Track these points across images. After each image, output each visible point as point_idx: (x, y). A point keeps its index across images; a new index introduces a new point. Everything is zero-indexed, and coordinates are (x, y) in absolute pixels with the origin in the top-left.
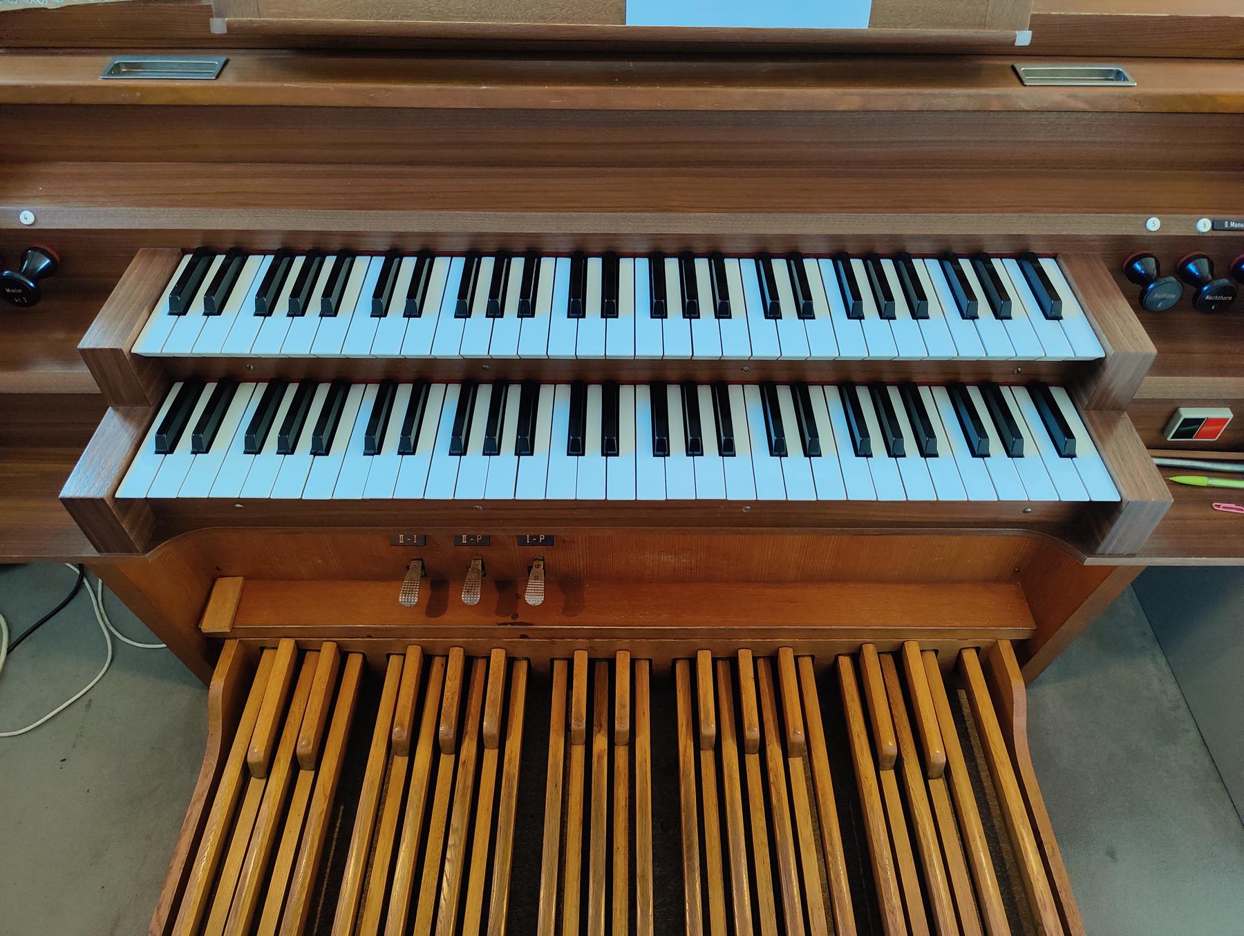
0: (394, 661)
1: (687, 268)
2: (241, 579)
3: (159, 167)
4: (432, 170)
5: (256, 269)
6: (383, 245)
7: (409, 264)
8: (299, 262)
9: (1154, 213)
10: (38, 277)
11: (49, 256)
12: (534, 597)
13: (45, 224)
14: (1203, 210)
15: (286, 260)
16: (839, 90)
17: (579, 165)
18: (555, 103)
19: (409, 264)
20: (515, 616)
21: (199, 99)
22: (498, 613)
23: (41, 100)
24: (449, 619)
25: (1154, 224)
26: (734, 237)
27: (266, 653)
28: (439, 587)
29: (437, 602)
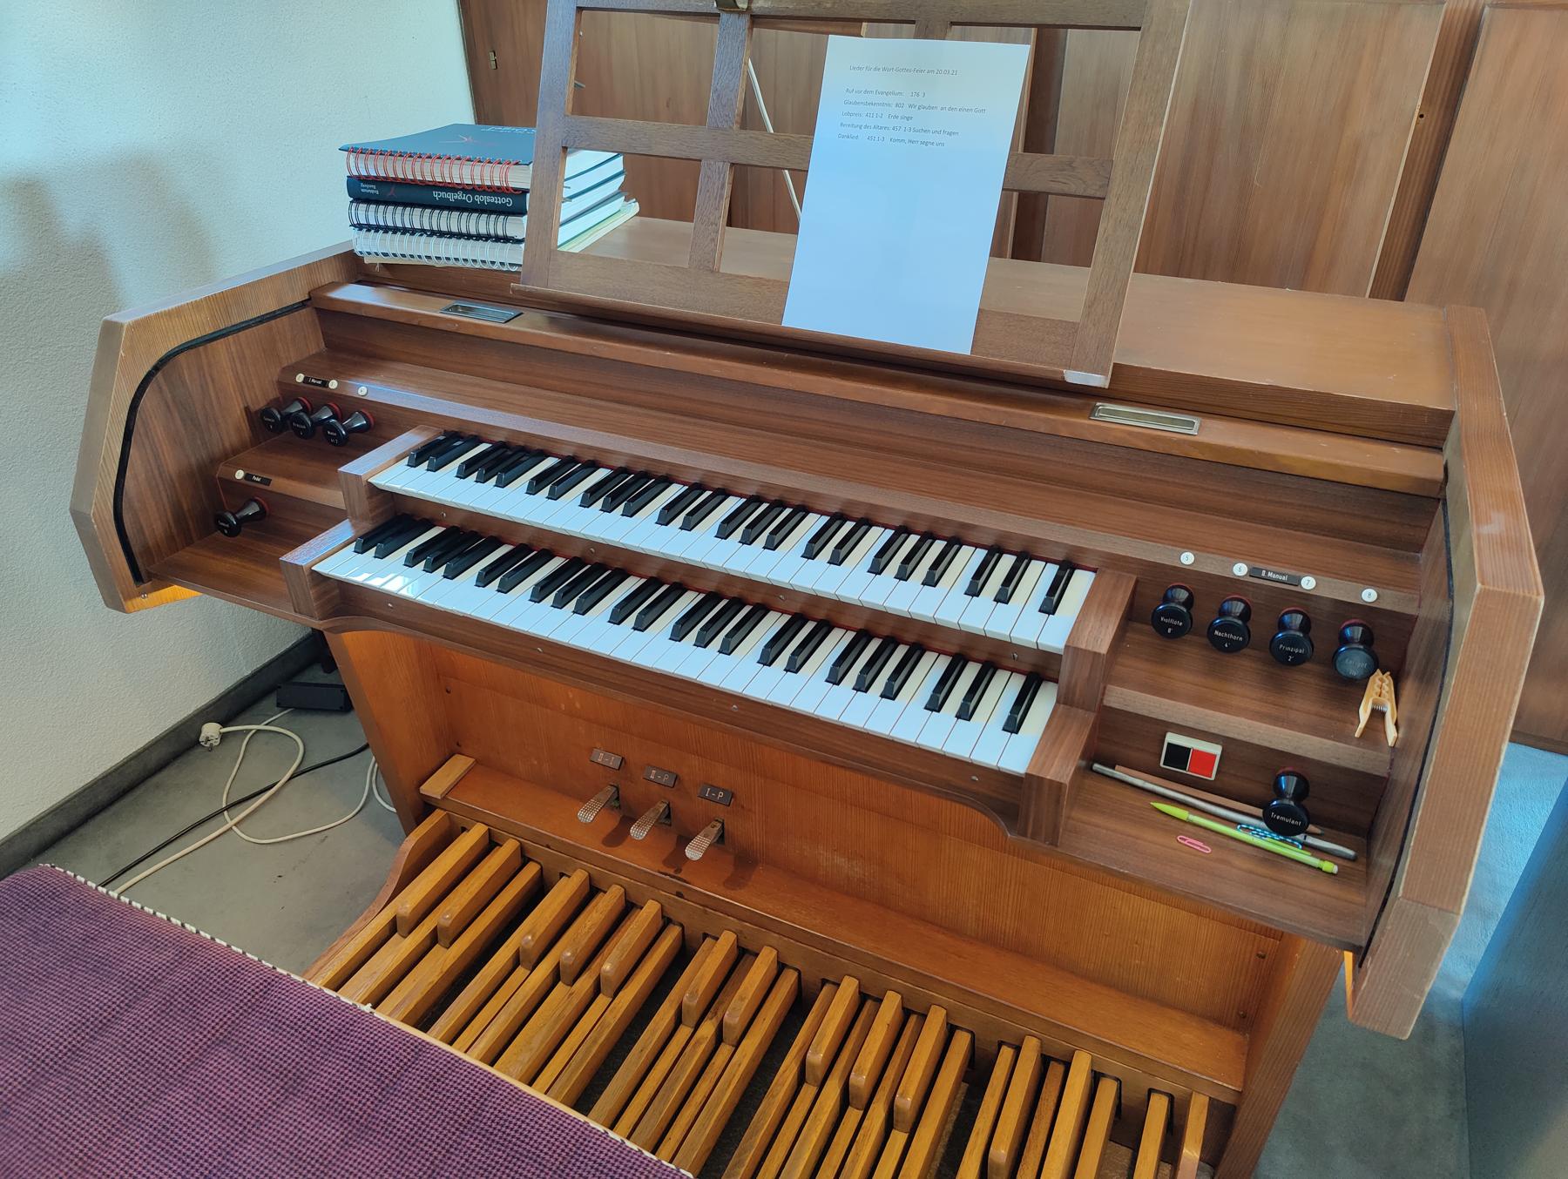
0: (1006, 1053)
1: (922, 542)
2: (471, 760)
3: (459, 377)
4: (630, 408)
5: (876, 538)
6: (989, 541)
7: (1007, 562)
8: (849, 526)
9: (1190, 549)
10: (350, 431)
11: (366, 418)
12: (693, 852)
13: (1326, 593)
14: (1311, 570)
15: (778, 509)
16: (929, 397)
17: (728, 422)
18: (717, 372)
19: (1007, 562)
20: (679, 871)
21: (492, 335)
22: (665, 862)
23: (351, 310)
24: (617, 854)
25: (1187, 558)
26: (891, 510)
27: (708, 940)
28: (625, 812)
29: (618, 836)
